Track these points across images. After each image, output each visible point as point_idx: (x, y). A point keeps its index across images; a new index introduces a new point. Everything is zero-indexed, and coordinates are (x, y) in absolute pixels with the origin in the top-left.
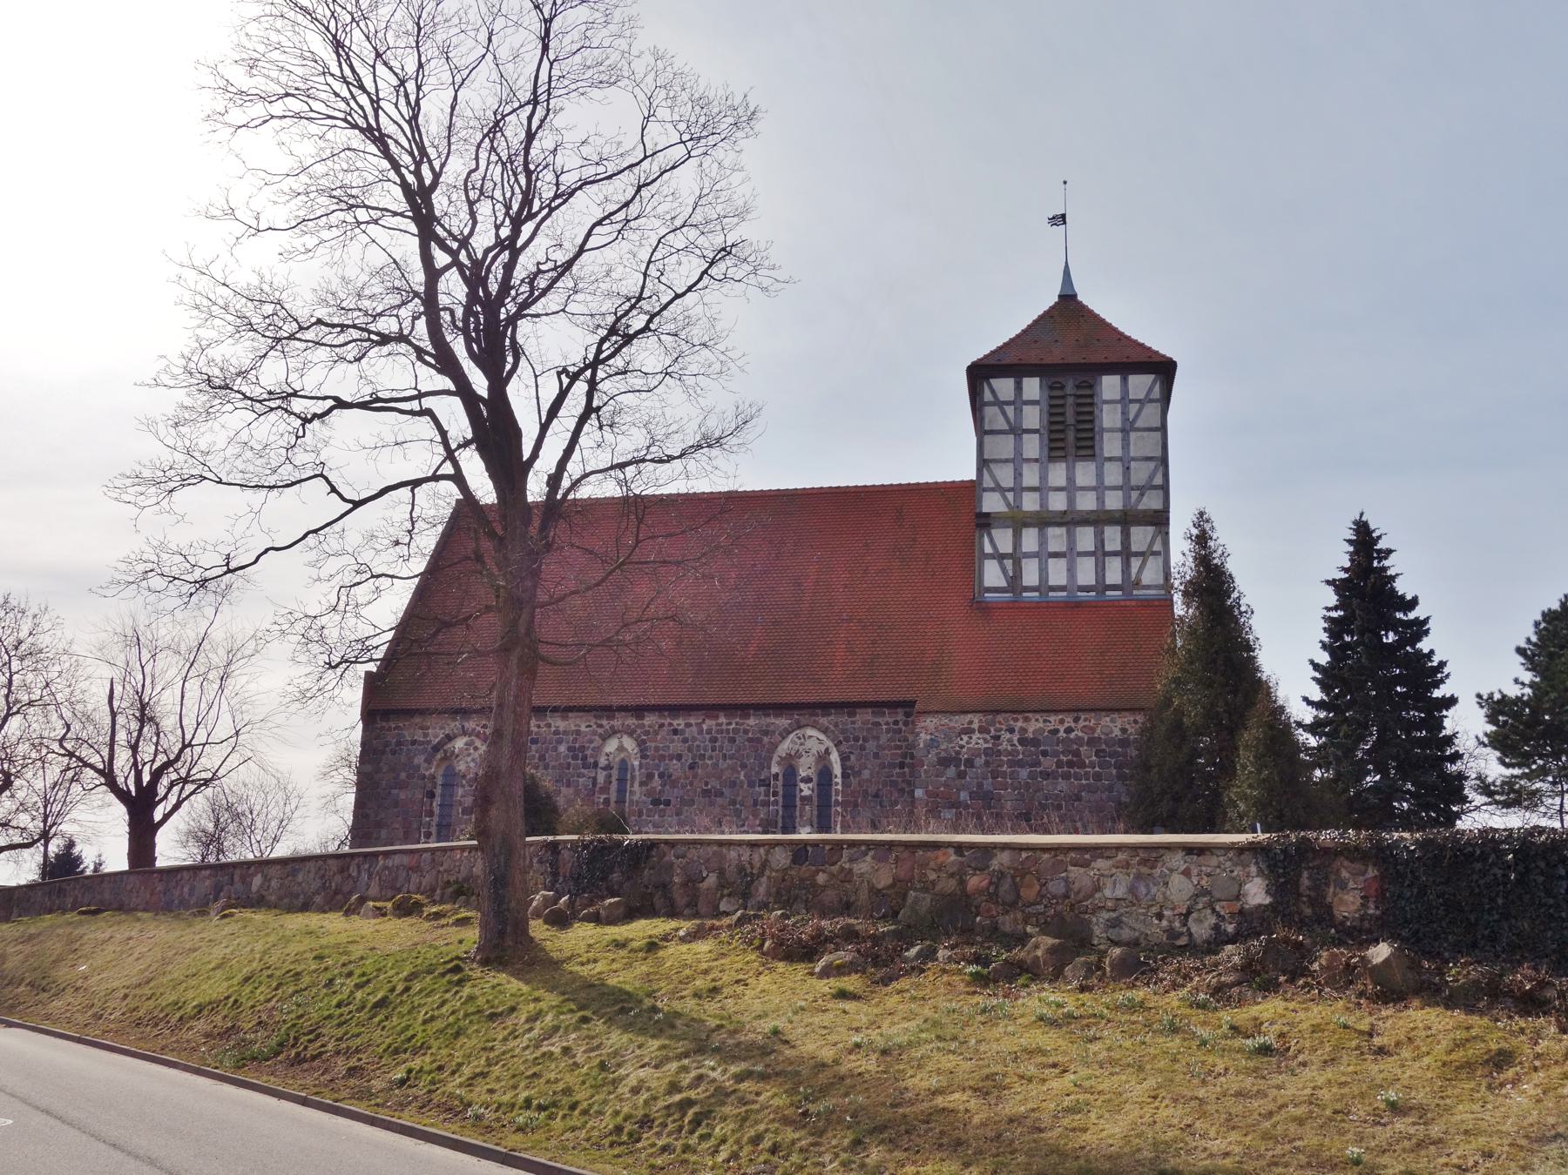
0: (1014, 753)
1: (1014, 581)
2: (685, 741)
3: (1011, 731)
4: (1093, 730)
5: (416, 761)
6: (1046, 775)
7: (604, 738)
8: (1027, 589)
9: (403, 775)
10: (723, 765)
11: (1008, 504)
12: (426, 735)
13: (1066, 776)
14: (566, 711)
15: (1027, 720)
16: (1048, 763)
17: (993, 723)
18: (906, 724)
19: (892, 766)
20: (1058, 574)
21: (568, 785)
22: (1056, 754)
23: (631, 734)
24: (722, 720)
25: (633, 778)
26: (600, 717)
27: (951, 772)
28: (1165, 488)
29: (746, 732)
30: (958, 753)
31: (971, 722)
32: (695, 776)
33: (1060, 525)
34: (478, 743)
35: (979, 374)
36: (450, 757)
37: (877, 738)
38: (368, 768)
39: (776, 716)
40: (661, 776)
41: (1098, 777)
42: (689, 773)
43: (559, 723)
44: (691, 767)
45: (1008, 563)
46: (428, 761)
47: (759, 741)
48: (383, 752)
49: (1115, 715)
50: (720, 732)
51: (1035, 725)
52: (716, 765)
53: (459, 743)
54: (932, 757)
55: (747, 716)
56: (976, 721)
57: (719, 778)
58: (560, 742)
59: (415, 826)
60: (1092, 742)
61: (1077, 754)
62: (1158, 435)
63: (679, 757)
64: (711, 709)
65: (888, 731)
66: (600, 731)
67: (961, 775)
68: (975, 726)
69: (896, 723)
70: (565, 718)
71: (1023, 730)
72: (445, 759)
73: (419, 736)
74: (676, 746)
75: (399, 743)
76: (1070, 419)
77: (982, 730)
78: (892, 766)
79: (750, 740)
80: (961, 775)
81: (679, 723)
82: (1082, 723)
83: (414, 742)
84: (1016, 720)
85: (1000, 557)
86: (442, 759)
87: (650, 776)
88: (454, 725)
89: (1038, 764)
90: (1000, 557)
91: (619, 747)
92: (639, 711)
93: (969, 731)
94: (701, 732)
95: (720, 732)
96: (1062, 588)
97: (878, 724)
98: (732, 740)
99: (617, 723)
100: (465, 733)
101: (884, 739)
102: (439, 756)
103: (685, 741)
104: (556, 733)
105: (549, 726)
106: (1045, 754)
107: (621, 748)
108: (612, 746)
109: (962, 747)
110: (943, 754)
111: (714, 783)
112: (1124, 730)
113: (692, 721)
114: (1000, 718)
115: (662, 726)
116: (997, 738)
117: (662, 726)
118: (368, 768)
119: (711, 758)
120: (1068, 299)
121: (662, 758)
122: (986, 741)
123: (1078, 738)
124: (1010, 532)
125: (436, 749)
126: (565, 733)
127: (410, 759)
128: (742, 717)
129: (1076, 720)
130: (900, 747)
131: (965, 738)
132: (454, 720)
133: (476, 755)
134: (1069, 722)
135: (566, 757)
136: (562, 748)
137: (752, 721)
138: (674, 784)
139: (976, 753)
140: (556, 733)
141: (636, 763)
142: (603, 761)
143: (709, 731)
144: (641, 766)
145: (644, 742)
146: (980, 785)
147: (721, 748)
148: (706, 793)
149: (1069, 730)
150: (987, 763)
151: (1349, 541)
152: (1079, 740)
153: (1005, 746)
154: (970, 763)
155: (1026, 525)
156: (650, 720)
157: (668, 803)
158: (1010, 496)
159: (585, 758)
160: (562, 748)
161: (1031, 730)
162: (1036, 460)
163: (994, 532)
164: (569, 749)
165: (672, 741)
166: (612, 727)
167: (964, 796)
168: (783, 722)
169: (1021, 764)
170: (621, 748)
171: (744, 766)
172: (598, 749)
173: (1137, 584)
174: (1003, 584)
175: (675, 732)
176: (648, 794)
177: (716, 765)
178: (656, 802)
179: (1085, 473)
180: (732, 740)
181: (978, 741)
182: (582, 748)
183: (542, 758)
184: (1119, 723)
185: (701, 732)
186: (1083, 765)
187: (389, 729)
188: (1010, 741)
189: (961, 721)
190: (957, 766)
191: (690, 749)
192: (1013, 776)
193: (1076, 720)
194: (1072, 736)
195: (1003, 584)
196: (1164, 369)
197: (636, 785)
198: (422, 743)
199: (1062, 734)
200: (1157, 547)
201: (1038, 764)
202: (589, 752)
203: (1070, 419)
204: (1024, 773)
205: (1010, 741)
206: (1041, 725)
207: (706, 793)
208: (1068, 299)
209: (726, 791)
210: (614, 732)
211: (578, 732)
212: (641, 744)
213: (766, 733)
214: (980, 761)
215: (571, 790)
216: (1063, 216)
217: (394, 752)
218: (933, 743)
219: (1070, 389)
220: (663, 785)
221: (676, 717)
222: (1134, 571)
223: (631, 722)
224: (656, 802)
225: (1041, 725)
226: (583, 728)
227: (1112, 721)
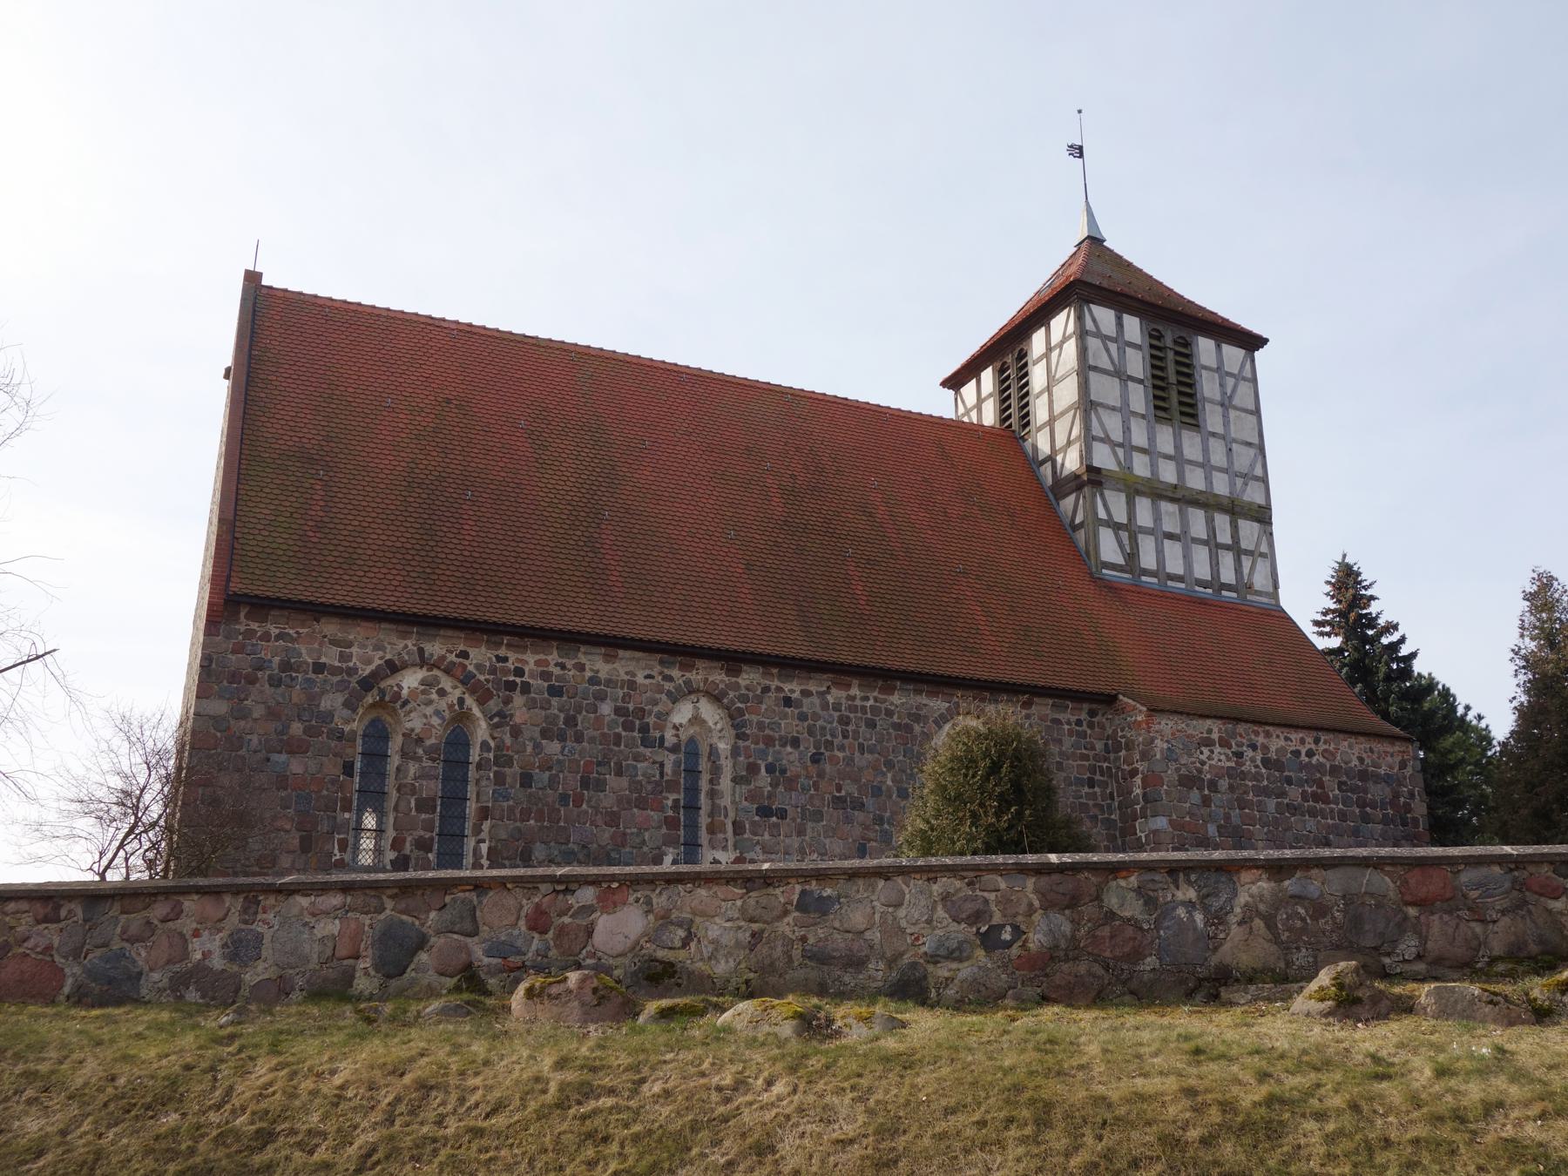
0: (1257, 777)
1: (1132, 556)
2: (803, 717)
3: (1254, 747)
4: (1333, 755)
5: (325, 704)
6: (1293, 809)
7: (675, 699)
8: (1146, 572)
9: (297, 728)
10: (861, 760)
11: (1119, 463)
12: (344, 657)
13: (1313, 813)
14: (612, 644)
15: (1268, 735)
16: (1294, 793)
17: (1234, 735)
18: (1091, 725)
19: (1079, 782)
20: (1175, 566)
21: (619, 773)
22: (1300, 783)
23: (717, 698)
24: (855, 691)
25: (716, 771)
26: (670, 665)
27: (1195, 796)
28: (1264, 480)
29: (889, 713)
30: (1200, 771)
31: (1210, 731)
32: (821, 775)
33: (1172, 500)
34: (446, 683)
35: (1097, 282)
36: (393, 703)
37: (1060, 742)
38: (219, 707)
39: (931, 694)
40: (770, 769)
41: (1343, 816)
42: (813, 770)
43: (596, 664)
44: (816, 759)
45: (1124, 535)
46: (350, 705)
47: (909, 728)
48: (252, 681)
49: (1352, 740)
50: (853, 709)
51: (1277, 742)
52: (849, 761)
53: (410, 680)
54: (1171, 774)
55: (889, 690)
56: (1216, 729)
57: (856, 780)
58: (601, 697)
59: (324, 827)
60: (1334, 770)
61: (1321, 785)
62: (1253, 419)
63: (795, 743)
64: (841, 671)
65: (1071, 733)
66: (668, 686)
67: (1206, 801)
68: (1215, 736)
69: (1079, 723)
70: (609, 658)
71: (1266, 748)
72: (379, 704)
73: (331, 657)
74: (789, 725)
75: (286, 666)
76: (1173, 378)
77: (1224, 743)
78: (1079, 782)
79: (897, 726)
80: (1206, 801)
81: (793, 688)
82: (1322, 747)
83: (319, 668)
84: (1257, 733)
85: (1117, 527)
86: (373, 706)
87: (753, 769)
88: (400, 645)
89: (1283, 794)
90: (1117, 527)
91: (693, 716)
92: (733, 660)
93: (1208, 743)
94: (825, 706)
95: (853, 709)
96: (1180, 579)
97: (1057, 722)
98: (871, 724)
99: (696, 677)
100: (423, 661)
101: (1068, 742)
102: (369, 699)
103: (803, 717)
104: (594, 681)
105: (581, 667)
106: (1289, 781)
107: (696, 720)
108: (682, 714)
109: (1203, 763)
110: (1183, 771)
111: (849, 788)
112: (1361, 760)
113: (813, 689)
114: (1241, 728)
115: (766, 689)
116: (1239, 755)
117: (766, 689)
118: (219, 707)
119: (842, 748)
120: (1094, 242)
121: (769, 741)
122: (1229, 759)
123: (1321, 765)
124: (1123, 497)
125: (367, 684)
126: (609, 682)
127: (313, 699)
128: (883, 690)
129: (1317, 741)
130: (1086, 758)
131: (1206, 751)
132: (404, 635)
133: (443, 704)
134: (1310, 744)
135: (613, 723)
136: (606, 709)
137: (896, 699)
138: (791, 784)
139: (1221, 773)
140: (594, 681)
141: (723, 747)
142: (670, 738)
143: (837, 707)
144: (735, 752)
145: (741, 712)
146: (1227, 817)
147: (856, 732)
148: (839, 802)
149: (1310, 754)
150: (1231, 788)
151: (1328, 583)
152: (1320, 767)
153: (1247, 767)
154: (1213, 785)
155: (1138, 493)
156: (750, 677)
157: (782, 814)
158: (1120, 451)
159: (645, 729)
160: (606, 709)
161: (1273, 748)
162: (1143, 416)
163: (1107, 493)
164: (618, 711)
165: (785, 716)
166: (688, 683)
167: (1212, 830)
168: (938, 705)
169: (1265, 792)
170: (696, 720)
171: (890, 765)
172: (663, 716)
173: (1249, 587)
174: (1121, 561)
175: (788, 702)
176: (751, 797)
177: (849, 761)
178: (765, 812)
179: (1192, 446)
180: (871, 724)
181: (1219, 758)
182: (641, 713)
183: (571, 721)
184: (1356, 751)
185: (825, 706)
186: (1326, 801)
187: (266, 637)
188: (1253, 760)
189: (1199, 727)
190: (1201, 789)
191: (811, 732)
192: (1261, 807)
193: (1317, 741)
194: (1314, 760)
195: (1121, 561)
196: (1252, 342)
197: (725, 783)
198: (335, 671)
199: (1304, 758)
200: (1264, 548)
201: (1283, 794)
202: (651, 720)
203: (1173, 378)
204: (1271, 804)
205: (1253, 760)
206: (1282, 743)
207: (839, 802)
208: (1094, 242)
209: (869, 802)
210: (690, 690)
211: (632, 685)
212: (735, 718)
213: (917, 718)
214: (1224, 784)
215: (624, 782)
216: (1081, 148)
217: (275, 682)
218: (1170, 756)
219: (1168, 341)
220: (774, 785)
221: (788, 678)
222: (1246, 571)
223: (719, 677)
224: (765, 812)
225: (1282, 743)
226: (640, 679)
227: (1350, 746)
